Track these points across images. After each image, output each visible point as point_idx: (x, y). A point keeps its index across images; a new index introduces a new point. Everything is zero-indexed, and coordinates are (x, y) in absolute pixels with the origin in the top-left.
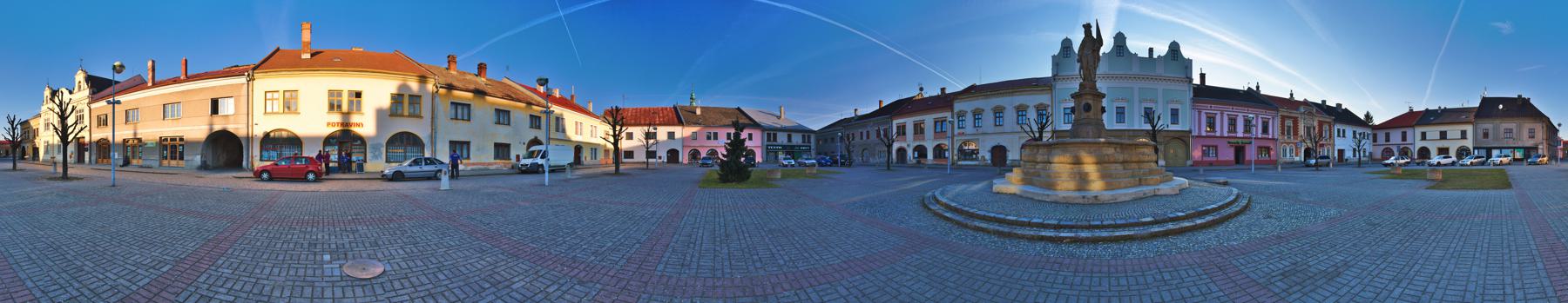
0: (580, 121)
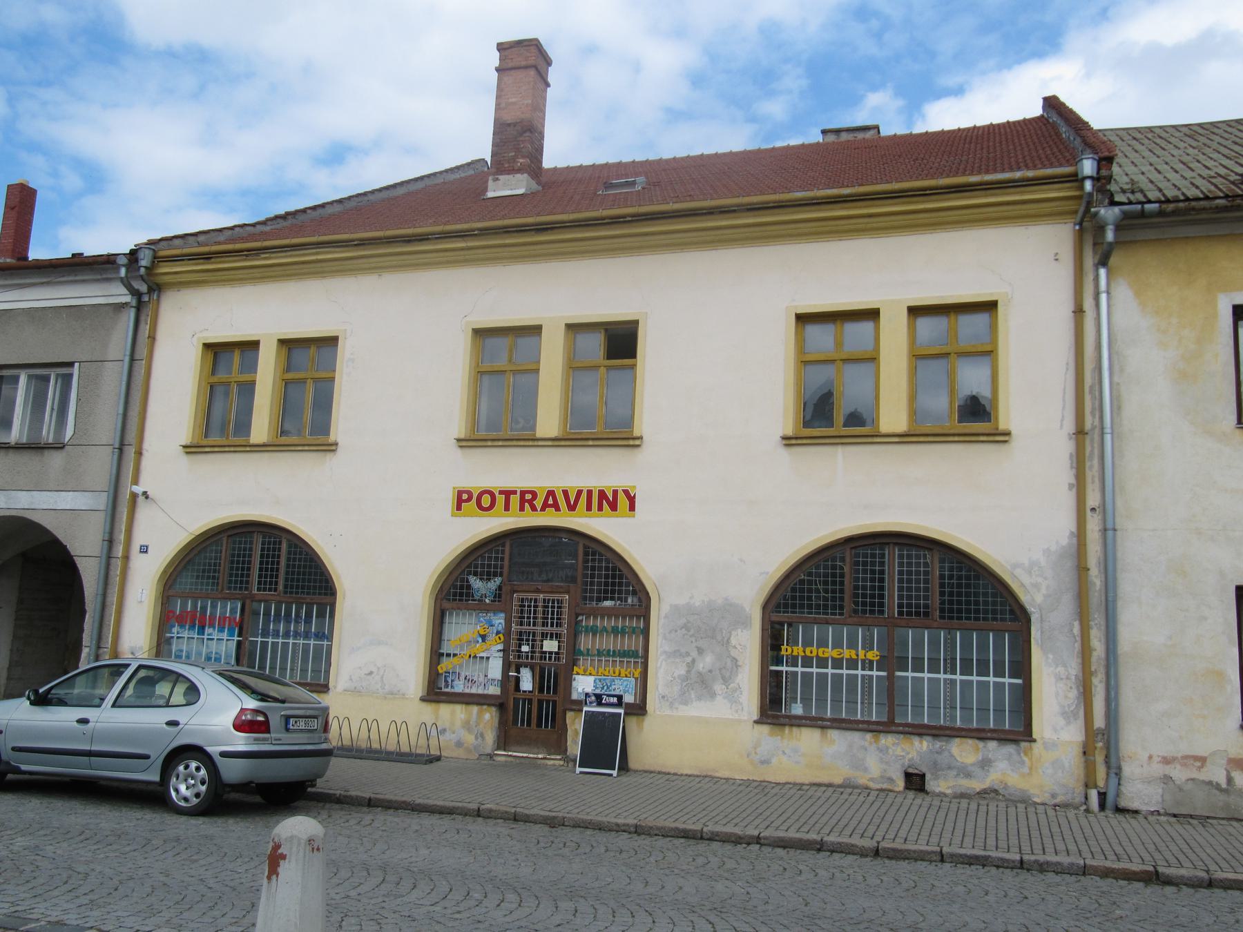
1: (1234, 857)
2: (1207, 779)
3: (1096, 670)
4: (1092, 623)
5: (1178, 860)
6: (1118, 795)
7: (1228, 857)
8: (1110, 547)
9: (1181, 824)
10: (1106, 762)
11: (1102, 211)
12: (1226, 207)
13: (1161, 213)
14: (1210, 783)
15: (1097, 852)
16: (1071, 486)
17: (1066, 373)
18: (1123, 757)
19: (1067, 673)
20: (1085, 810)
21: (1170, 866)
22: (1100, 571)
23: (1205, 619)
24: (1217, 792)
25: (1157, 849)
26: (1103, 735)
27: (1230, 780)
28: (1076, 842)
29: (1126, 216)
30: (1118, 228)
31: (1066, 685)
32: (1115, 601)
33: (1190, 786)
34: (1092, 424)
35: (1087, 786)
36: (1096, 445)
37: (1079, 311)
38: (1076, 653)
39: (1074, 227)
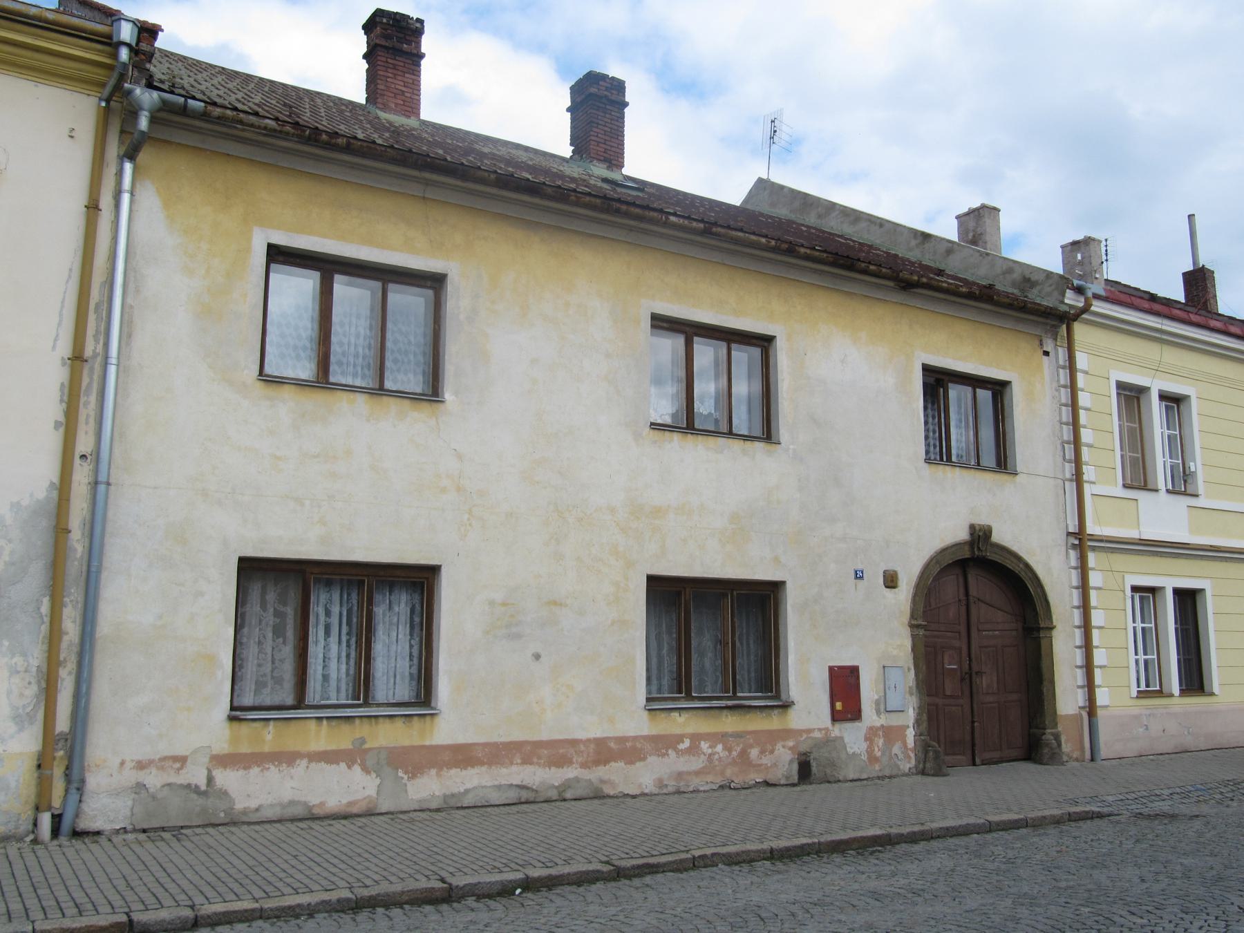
0: (1156, 385)
1: (219, 879)
2: (185, 782)
3: (65, 659)
4: (66, 600)
5: (157, 898)
6: (77, 816)
7: (211, 878)
8: (100, 504)
9: (153, 841)
10: (66, 775)
11: (138, 91)
12: (275, 130)
13: (204, 116)
14: (188, 786)
15: (50, 906)
16: (57, 425)
17: (67, 282)
18: (89, 765)
19: (25, 665)
20: (31, 841)
21: (147, 910)
22: (83, 534)
23: (201, 594)
24: (194, 796)
25: (128, 885)
26: (66, 740)
27: (210, 780)
28: (20, 895)
29: (165, 106)
30: (153, 120)
31: (23, 679)
32: (99, 572)
33: (166, 791)
34: (94, 351)
35: (37, 809)
36: (95, 377)
37: (93, 207)
38: (41, 638)
39: (99, 104)
